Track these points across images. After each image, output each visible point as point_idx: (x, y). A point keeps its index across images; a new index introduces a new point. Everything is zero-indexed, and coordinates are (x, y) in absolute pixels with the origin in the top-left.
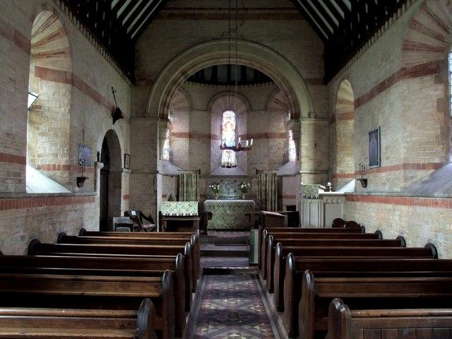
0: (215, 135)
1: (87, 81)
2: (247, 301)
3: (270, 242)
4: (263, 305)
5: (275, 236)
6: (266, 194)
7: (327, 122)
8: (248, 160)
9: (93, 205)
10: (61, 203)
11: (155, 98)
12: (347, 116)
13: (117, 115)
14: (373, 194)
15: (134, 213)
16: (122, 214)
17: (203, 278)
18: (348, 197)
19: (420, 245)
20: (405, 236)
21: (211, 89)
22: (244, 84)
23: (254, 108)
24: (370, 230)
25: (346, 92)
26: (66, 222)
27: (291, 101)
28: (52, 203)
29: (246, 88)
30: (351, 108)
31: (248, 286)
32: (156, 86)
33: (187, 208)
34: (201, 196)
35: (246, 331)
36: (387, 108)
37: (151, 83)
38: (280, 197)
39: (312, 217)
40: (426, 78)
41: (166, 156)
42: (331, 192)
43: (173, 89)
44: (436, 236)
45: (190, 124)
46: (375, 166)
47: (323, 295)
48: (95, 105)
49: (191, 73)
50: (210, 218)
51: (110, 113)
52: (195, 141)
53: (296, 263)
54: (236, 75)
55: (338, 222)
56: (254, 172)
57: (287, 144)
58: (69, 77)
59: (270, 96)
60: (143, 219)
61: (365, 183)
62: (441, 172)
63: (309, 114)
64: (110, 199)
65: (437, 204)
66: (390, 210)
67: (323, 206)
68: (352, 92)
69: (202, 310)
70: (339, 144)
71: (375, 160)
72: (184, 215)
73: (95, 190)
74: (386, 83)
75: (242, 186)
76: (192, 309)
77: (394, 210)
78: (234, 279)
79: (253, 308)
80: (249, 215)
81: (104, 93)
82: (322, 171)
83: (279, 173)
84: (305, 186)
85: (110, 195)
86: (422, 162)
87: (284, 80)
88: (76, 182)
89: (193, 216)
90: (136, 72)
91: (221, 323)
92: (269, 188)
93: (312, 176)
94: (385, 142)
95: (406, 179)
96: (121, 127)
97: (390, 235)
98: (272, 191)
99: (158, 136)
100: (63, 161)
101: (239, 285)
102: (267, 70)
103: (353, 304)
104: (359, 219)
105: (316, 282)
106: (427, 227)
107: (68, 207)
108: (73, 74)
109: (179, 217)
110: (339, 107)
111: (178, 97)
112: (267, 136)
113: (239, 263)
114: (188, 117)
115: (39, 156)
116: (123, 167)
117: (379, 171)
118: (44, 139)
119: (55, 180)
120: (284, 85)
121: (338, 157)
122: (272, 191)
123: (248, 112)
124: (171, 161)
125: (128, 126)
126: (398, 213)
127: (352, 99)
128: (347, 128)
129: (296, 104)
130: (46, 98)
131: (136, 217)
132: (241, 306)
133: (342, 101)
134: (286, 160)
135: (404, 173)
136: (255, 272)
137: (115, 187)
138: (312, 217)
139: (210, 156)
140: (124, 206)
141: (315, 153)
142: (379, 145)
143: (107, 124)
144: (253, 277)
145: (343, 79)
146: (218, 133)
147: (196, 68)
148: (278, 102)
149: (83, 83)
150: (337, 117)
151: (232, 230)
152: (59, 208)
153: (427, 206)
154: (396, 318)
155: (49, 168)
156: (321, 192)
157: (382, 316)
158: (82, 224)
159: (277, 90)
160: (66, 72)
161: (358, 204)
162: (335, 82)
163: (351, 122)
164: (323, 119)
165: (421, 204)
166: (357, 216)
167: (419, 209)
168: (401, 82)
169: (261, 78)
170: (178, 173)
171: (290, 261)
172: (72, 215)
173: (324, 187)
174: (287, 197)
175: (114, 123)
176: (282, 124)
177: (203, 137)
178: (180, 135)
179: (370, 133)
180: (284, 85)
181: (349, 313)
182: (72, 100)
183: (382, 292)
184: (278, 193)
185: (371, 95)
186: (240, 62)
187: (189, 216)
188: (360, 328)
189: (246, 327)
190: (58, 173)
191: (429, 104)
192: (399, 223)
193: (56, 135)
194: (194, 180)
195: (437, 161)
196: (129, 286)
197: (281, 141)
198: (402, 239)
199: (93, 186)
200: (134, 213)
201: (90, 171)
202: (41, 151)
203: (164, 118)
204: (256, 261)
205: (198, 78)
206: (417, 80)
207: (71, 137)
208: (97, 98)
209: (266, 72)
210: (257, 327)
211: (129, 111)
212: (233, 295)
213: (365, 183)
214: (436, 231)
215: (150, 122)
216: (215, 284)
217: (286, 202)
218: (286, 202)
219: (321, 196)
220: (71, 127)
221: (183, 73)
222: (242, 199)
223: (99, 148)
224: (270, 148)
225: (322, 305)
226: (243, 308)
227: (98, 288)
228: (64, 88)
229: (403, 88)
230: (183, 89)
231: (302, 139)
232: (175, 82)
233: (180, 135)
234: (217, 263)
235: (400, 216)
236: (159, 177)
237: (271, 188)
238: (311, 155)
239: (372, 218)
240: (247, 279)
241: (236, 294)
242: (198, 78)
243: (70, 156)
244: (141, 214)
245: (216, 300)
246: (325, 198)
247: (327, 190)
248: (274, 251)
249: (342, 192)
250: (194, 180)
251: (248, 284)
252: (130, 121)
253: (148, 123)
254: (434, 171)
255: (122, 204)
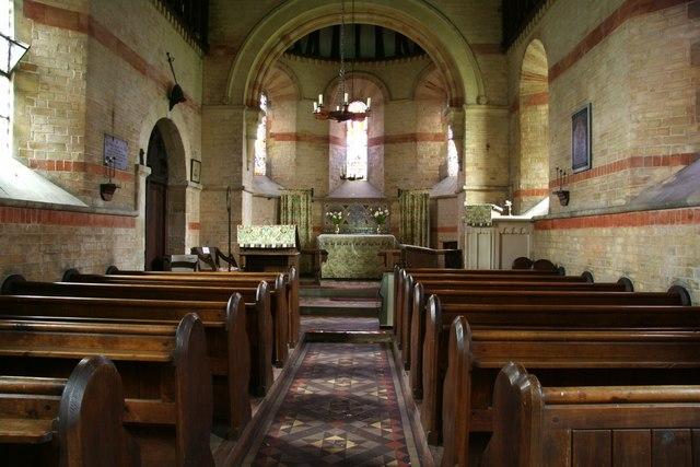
0: (336, 138)
1: (121, 35)
2: (368, 382)
3: (418, 294)
4: (393, 389)
5: (426, 286)
6: (412, 227)
7: (506, 111)
8: (386, 174)
9: (131, 231)
10: (70, 222)
11: (242, 73)
12: (535, 100)
13: (175, 96)
14: (578, 214)
15: (206, 250)
16: (188, 251)
17: (302, 348)
18: (539, 224)
19: (659, 287)
20: (632, 277)
21: (326, 68)
22: (381, 60)
23: (394, 96)
24: (573, 271)
25: (536, 59)
26: (78, 253)
27: (451, 79)
28: (51, 220)
29: (379, 67)
30: (544, 87)
31: (374, 361)
32: (241, 55)
33: (279, 236)
34: (314, 229)
35: (359, 431)
36: (603, 70)
37: (233, 52)
38: (434, 230)
39: (480, 255)
40: (672, 11)
41: (261, 168)
42: (511, 217)
43: (267, 64)
44: (689, 272)
45: (297, 119)
46: (582, 169)
47: (484, 364)
48: (136, 76)
49: (295, 37)
50: (325, 260)
51: (164, 92)
52: (305, 146)
53: (443, 311)
54: (368, 44)
55: (522, 263)
56: (394, 193)
57: (445, 151)
58: (84, 22)
59: (419, 79)
60: (221, 259)
61: (565, 197)
62: (690, 171)
63: (478, 98)
64: (169, 229)
65: (690, 217)
66: (607, 238)
67: (498, 238)
68: (545, 60)
69: (289, 396)
70: (524, 144)
71: (583, 162)
72: (274, 246)
73: (136, 208)
74: (603, 30)
75: (377, 214)
76: (268, 395)
77: (614, 236)
78: (352, 350)
79: (376, 394)
80: (385, 255)
81: (152, 58)
82: (499, 188)
83: (432, 194)
84: (470, 207)
85: (169, 220)
86: (663, 153)
87: (441, 47)
88: (98, 191)
89: (287, 249)
90: (211, 36)
91: (316, 417)
92: (417, 217)
93: (482, 194)
94: (598, 127)
95: (635, 183)
96: (185, 118)
97: (607, 275)
98: (421, 220)
99: (244, 133)
100: (75, 155)
101: (358, 358)
102: (414, 32)
103: (550, 378)
104: (555, 255)
105: (474, 339)
106: (671, 259)
107: (84, 230)
108: (90, 17)
109: (265, 249)
110: (525, 86)
111: (275, 77)
112: (414, 138)
113: (365, 327)
114: (295, 109)
115: (34, 146)
116: (188, 178)
117: (588, 176)
118: (41, 120)
119: (60, 186)
120: (439, 55)
121: (522, 163)
122: (421, 220)
123: (388, 99)
124: (269, 175)
125: (198, 117)
126: (620, 240)
127: (545, 72)
128: (538, 119)
129: (458, 84)
130: (45, 54)
131: (209, 255)
132: (357, 390)
133: (530, 76)
134: (443, 175)
135: (632, 173)
136: (388, 340)
137: (175, 210)
138: (480, 255)
139: (328, 169)
140: (191, 239)
141: (487, 160)
142: (588, 134)
143: (158, 109)
144: (383, 346)
145: (531, 41)
146: (340, 135)
147: (302, 29)
148: (431, 86)
149: (112, 36)
150: (522, 101)
151: (360, 279)
152: (65, 229)
153: (672, 222)
154: (647, 406)
155: (50, 166)
156: (495, 215)
157: (615, 400)
158: (112, 260)
159: (431, 66)
160: (78, 14)
161: (554, 233)
162: (517, 46)
163: (544, 108)
164: (500, 106)
165: (662, 222)
166: (552, 252)
167: (657, 230)
168: (627, 22)
169: (407, 49)
170: (280, 193)
171: (433, 308)
172: (89, 244)
173: (501, 210)
174: (444, 230)
175: (171, 108)
176: (436, 122)
177: (318, 141)
178: (282, 137)
179: (574, 117)
180: (439, 55)
181: (540, 392)
182: (89, 58)
183: (601, 358)
184: (431, 224)
185: (576, 55)
186: (372, 20)
187: (280, 249)
188: (565, 427)
189: (358, 424)
190: (66, 175)
191: (678, 56)
192: (622, 256)
193: (62, 114)
194: (303, 205)
195: (689, 150)
196: (116, 341)
197: (436, 146)
198: (627, 284)
199: (132, 202)
200: (206, 250)
201: (125, 177)
202: (37, 138)
203: (254, 106)
204: (390, 323)
205: (308, 48)
206: (657, 15)
207: (88, 118)
208: (140, 66)
209: (412, 35)
210: (378, 425)
211: (200, 95)
212: (347, 372)
213: (565, 197)
214: (688, 265)
215: (229, 113)
216: (321, 356)
217: (443, 237)
218: (443, 237)
219: (496, 222)
220: (89, 102)
221: (284, 37)
222: (375, 232)
223: (144, 143)
224: (416, 156)
225: (485, 379)
226: (359, 394)
227: (61, 343)
228: (75, 39)
229: (633, 31)
230: (282, 66)
231: (467, 136)
232: (271, 50)
233: (282, 137)
234: (330, 325)
235: (624, 246)
236: (247, 198)
237: (420, 216)
238: (481, 163)
239: (577, 253)
240: (373, 350)
241: (351, 372)
242: (308, 48)
243: (87, 149)
244: (218, 253)
245: (317, 381)
246: (502, 226)
247: (505, 212)
248: (424, 313)
249: (528, 216)
250: (303, 205)
251: (375, 356)
252: (201, 110)
253: (227, 113)
254: (682, 167)
255: (187, 237)
